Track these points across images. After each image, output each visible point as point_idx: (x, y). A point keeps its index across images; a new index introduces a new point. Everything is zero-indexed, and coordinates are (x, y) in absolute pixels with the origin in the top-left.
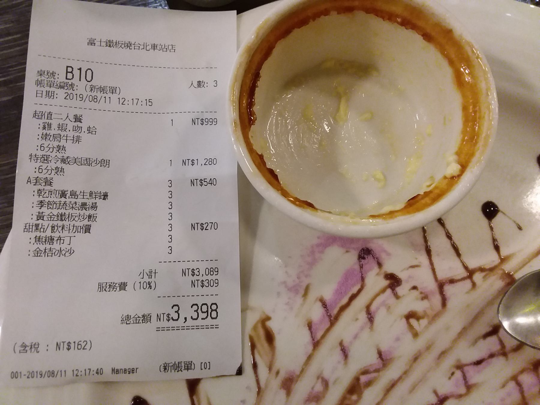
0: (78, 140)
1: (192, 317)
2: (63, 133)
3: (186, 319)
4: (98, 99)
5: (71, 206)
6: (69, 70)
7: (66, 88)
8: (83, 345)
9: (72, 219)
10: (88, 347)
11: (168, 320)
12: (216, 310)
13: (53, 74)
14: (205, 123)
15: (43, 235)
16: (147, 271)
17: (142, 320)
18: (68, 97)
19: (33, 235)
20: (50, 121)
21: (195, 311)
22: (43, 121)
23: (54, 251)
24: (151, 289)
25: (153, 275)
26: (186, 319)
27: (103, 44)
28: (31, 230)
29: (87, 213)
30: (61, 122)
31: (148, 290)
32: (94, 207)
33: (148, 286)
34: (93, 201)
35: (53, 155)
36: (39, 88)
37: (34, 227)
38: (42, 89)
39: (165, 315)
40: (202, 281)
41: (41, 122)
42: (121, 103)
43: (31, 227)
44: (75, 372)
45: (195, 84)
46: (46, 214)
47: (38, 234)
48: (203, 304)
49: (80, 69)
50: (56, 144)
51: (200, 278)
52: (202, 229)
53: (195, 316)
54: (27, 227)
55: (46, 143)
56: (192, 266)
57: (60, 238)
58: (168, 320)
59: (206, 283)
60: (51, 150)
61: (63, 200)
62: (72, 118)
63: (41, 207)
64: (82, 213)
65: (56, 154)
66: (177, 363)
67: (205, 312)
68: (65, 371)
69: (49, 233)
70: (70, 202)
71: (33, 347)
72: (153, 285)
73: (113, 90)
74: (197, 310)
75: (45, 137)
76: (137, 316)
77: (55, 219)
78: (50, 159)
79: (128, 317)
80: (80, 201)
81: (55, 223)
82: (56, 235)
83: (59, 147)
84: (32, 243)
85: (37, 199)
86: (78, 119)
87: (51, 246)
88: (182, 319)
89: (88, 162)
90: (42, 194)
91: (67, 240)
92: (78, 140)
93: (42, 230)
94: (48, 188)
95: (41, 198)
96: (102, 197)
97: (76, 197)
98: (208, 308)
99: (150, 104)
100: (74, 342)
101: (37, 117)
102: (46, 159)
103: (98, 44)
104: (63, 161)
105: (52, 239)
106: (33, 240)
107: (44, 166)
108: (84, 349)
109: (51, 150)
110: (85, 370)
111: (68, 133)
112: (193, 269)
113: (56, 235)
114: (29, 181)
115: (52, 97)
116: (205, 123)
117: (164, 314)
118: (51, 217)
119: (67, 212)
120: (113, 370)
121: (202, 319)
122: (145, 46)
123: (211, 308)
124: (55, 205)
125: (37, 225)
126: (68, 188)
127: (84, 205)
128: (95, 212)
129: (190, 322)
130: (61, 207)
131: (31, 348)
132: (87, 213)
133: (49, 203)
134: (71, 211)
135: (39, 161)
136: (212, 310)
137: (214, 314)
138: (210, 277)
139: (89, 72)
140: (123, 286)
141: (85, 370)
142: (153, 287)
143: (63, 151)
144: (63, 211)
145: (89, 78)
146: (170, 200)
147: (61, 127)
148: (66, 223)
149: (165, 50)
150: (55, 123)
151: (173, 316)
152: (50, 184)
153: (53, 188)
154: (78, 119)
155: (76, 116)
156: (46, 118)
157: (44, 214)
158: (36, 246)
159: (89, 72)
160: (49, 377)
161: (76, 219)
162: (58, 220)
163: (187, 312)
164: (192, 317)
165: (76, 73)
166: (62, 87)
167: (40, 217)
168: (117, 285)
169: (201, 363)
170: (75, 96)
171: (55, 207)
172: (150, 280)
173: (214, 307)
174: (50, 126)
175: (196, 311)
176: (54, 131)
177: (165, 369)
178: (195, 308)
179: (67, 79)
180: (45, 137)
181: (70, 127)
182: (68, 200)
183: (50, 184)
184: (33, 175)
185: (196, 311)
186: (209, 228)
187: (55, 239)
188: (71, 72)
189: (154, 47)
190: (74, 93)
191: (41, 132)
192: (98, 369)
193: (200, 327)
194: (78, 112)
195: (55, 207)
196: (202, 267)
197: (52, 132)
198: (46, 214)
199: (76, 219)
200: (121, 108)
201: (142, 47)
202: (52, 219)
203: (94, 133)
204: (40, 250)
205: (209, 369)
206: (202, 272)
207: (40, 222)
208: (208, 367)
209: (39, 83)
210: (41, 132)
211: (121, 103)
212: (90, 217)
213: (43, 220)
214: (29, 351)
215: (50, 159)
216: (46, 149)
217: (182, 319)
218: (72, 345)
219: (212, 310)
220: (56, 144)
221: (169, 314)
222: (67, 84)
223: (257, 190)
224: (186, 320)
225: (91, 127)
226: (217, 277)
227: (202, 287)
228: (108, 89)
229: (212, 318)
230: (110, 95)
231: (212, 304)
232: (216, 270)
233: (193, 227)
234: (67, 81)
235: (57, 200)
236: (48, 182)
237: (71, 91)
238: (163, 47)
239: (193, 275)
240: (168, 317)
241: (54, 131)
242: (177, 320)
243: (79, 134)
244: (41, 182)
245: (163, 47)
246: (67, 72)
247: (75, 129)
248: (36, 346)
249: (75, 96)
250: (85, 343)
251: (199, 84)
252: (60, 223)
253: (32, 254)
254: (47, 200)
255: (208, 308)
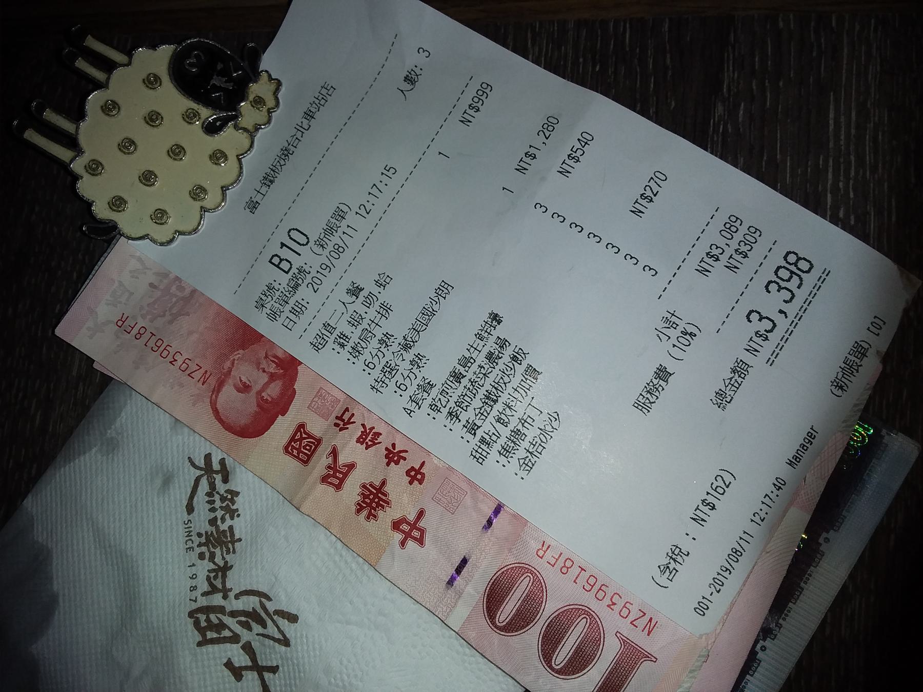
0: (386, 309)
1: (786, 302)
2: (365, 325)
3: (781, 312)
4: (342, 244)
5: (481, 376)
6: (276, 262)
7: (300, 282)
8: (648, 193)
9: (503, 386)
10: (728, 478)
11: (767, 339)
12: (799, 259)
13: (270, 288)
14: (479, 105)
15: (502, 441)
16: (661, 325)
17: (740, 376)
18: (316, 287)
19: (494, 454)
20: (337, 332)
21: (779, 291)
22: (331, 341)
23: (537, 439)
24: (695, 335)
25: (674, 319)
26: (781, 312)
27: (264, 190)
28: (484, 453)
29: (506, 359)
30: (347, 317)
31: (695, 341)
32: (503, 343)
33: (688, 337)
34: (492, 339)
35: (389, 356)
36: (280, 320)
37: (482, 446)
38: (284, 316)
39: (755, 339)
40: (736, 251)
41: (330, 344)
42: (364, 214)
43: (480, 451)
44: (757, 519)
45: (406, 86)
46: (473, 418)
47: (497, 447)
48: (776, 273)
49: (283, 245)
50: (374, 343)
51: (729, 251)
52: (651, 201)
53: (788, 296)
54: (478, 455)
55: (366, 356)
56: (700, 251)
57: (523, 421)
58: (767, 339)
59: (744, 248)
60: (380, 354)
61: (465, 381)
62: (348, 299)
63: (457, 418)
64: (501, 366)
65: (391, 351)
66: (843, 365)
67: (791, 277)
68: (745, 532)
69: (505, 432)
70: (475, 373)
71: (674, 556)
72: (690, 329)
73: (340, 215)
74: (779, 286)
75: (356, 351)
76: (727, 382)
77: (488, 409)
78: (393, 365)
79: (720, 394)
80: (481, 359)
81: (494, 413)
82: (514, 423)
83: (381, 341)
84: (506, 463)
85: (442, 416)
86: (355, 291)
87: (527, 439)
88: (779, 319)
89: (428, 314)
90: (440, 406)
91: (534, 413)
92: (386, 309)
93: (494, 438)
94: (434, 392)
95: (445, 411)
96: (495, 323)
97: (472, 361)
98: (788, 269)
99: (392, 171)
100: (708, 493)
101: (320, 347)
102: (389, 370)
103: (258, 198)
104: (406, 347)
105: (517, 432)
106: (503, 460)
107: (398, 377)
108: (727, 487)
109: (380, 354)
110: (763, 503)
111: (368, 317)
112: (708, 254)
113: (514, 423)
114: (410, 412)
115: (303, 309)
116: (479, 105)
117: (751, 339)
118: (481, 414)
119: (488, 387)
120: (790, 463)
121: (799, 287)
122: (300, 129)
123: (790, 264)
124: (466, 398)
125: (483, 440)
126: (452, 363)
127: (490, 356)
128: (512, 348)
129: (792, 309)
130: (474, 391)
131: (675, 560)
132: (506, 359)
133: (458, 404)
134: (489, 381)
135: (387, 381)
136: (796, 264)
137: (804, 265)
138: (738, 237)
139: (294, 234)
140: (663, 374)
141: (763, 503)
142: (695, 331)
143: (392, 339)
144: (482, 392)
145: (303, 240)
146: (567, 222)
147: (355, 321)
148: (504, 398)
149: (323, 102)
150: (343, 327)
151: (763, 326)
152: (432, 386)
153: (439, 386)
154: (355, 291)
155: (349, 291)
156: (329, 334)
157: (470, 421)
158: (514, 461)
159: (294, 234)
160: (738, 561)
161: (506, 379)
162: (492, 407)
163: (771, 303)
164: (786, 302)
165: (285, 253)
166: (296, 287)
167: (472, 429)
168: (655, 381)
169: (868, 329)
170: (319, 276)
171: (469, 400)
172: (680, 329)
173: (792, 258)
174: (343, 336)
175: (780, 288)
176: (355, 335)
177: (841, 388)
178: (773, 287)
179: (287, 273)
180: (356, 351)
181: (361, 309)
182: (470, 375)
183: (432, 386)
184: (404, 401)
185: (780, 288)
186: (655, 188)
187: (520, 427)
188: (281, 260)
189: (309, 115)
190: (314, 273)
191: (345, 353)
192: (774, 485)
193: (810, 298)
194: (346, 284)
195: (469, 400)
196: (713, 236)
197: (355, 339)
198: (473, 418)
199: (506, 379)
200: (373, 218)
201: (299, 134)
202: (485, 414)
203: (388, 280)
204: (525, 459)
205: (885, 323)
206: (721, 242)
207: (480, 433)
208: (881, 323)
209: (273, 316)
210: (345, 353)
211: (364, 214)
212: (514, 358)
213: (479, 427)
214: (678, 567)
215: (393, 365)
216: (376, 360)
217: (779, 319)
218: (710, 499)
219: (796, 264)
220: (374, 343)
221: (757, 333)
222: (295, 276)
223: (745, 658)
224: (785, 313)
225: (377, 278)
226: (745, 226)
227: (746, 256)
228: (333, 221)
229: (808, 272)
230: (344, 223)
231: (785, 258)
232: (733, 219)
233: (637, 212)
234: (291, 273)
235: (461, 390)
236: (427, 387)
237: (309, 277)
238: (317, 102)
239: (717, 260)
240: (761, 336)
241: (355, 335)
242: (775, 325)
243: (379, 301)
244: (419, 396)
245: (317, 102)
246: (278, 266)
247: (368, 303)
248: (676, 552)
249: (319, 276)
250: (719, 478)
251: (410, 79)
252: (499, 406)
253: (523, 474)
254: (452, 404)
255: (788, 269)
